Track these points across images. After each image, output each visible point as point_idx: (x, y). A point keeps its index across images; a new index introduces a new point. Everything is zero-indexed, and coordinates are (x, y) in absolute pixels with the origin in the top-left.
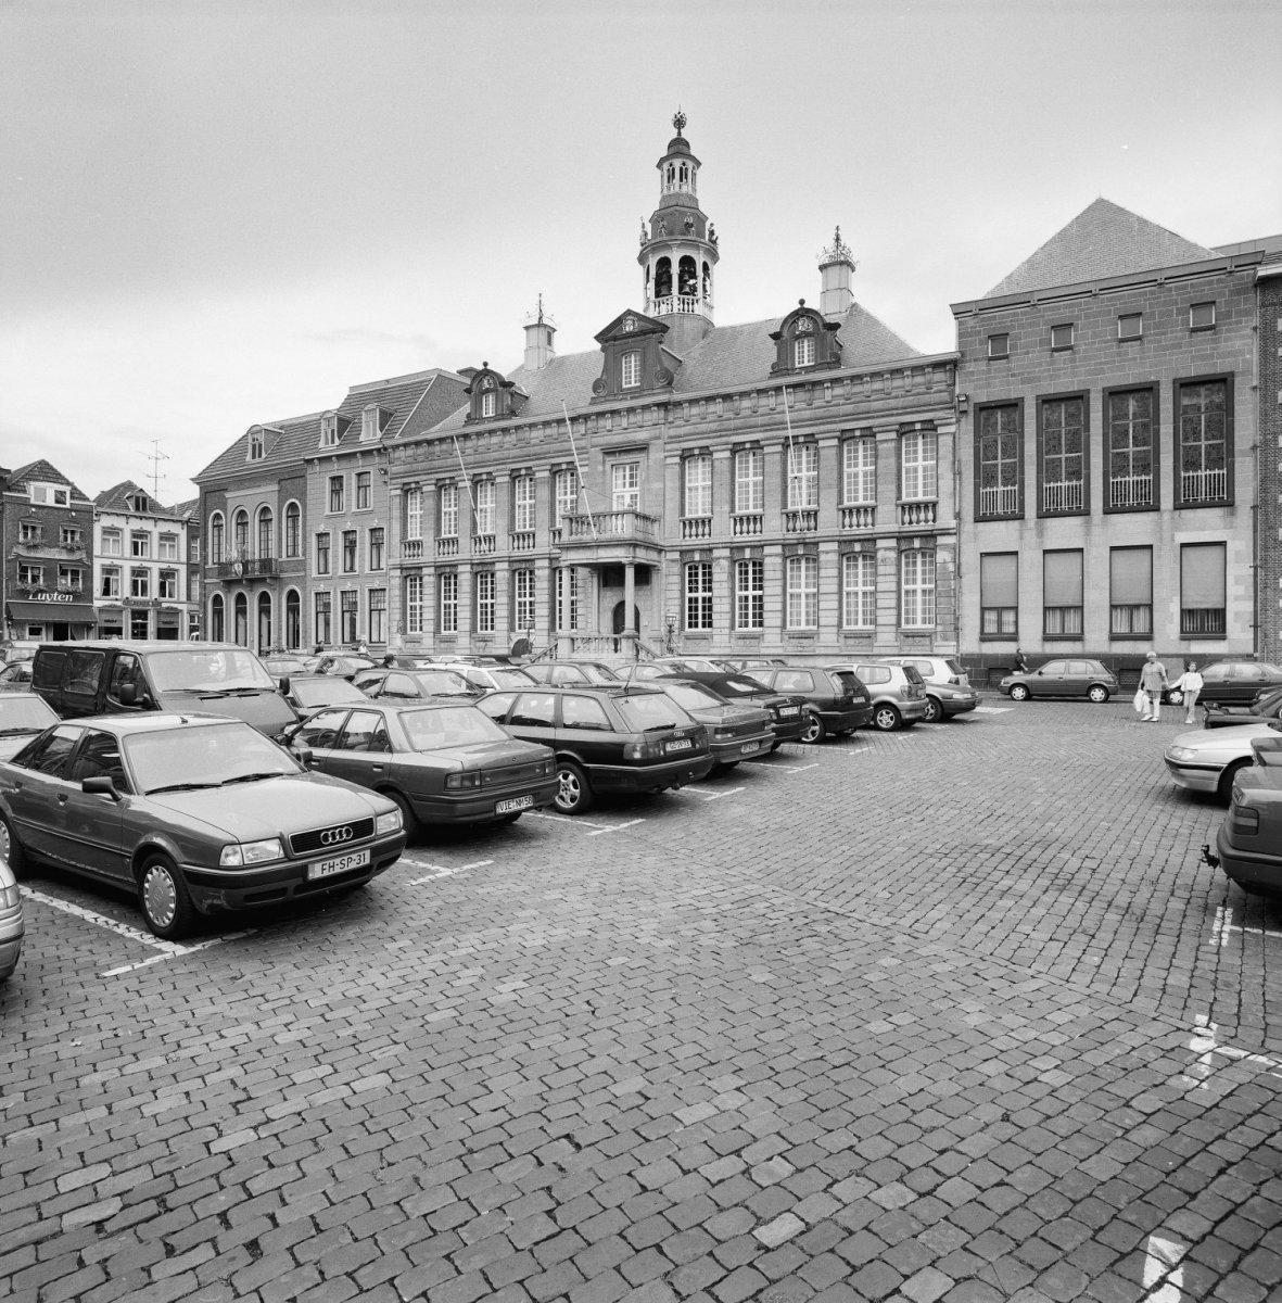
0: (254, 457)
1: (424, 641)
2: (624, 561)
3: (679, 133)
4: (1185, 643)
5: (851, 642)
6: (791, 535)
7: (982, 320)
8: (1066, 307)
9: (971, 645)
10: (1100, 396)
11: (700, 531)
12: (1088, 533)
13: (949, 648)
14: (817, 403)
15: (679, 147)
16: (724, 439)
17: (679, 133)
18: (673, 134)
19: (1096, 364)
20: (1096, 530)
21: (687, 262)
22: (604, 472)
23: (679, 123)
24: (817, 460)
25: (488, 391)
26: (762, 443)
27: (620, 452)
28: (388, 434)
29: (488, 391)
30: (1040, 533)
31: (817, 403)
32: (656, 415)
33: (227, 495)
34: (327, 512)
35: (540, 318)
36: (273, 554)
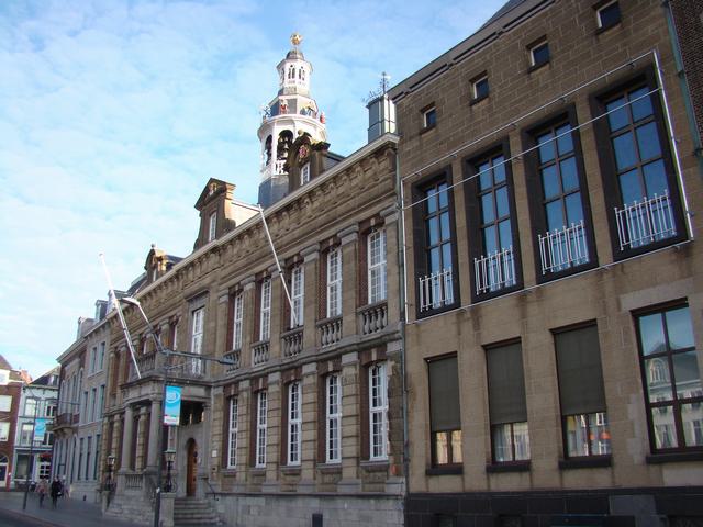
4: (654, 469)
7: (415, 97)
8: (479, 56)
9: (418, 483)
10: (586, 104)
12: (524, 316)
13: (397, 487)
14: (303, 220)
16: (249, 272)
19: (512, 105)
27: (196, 298)
31: (303, 220)
32: (214, 258)
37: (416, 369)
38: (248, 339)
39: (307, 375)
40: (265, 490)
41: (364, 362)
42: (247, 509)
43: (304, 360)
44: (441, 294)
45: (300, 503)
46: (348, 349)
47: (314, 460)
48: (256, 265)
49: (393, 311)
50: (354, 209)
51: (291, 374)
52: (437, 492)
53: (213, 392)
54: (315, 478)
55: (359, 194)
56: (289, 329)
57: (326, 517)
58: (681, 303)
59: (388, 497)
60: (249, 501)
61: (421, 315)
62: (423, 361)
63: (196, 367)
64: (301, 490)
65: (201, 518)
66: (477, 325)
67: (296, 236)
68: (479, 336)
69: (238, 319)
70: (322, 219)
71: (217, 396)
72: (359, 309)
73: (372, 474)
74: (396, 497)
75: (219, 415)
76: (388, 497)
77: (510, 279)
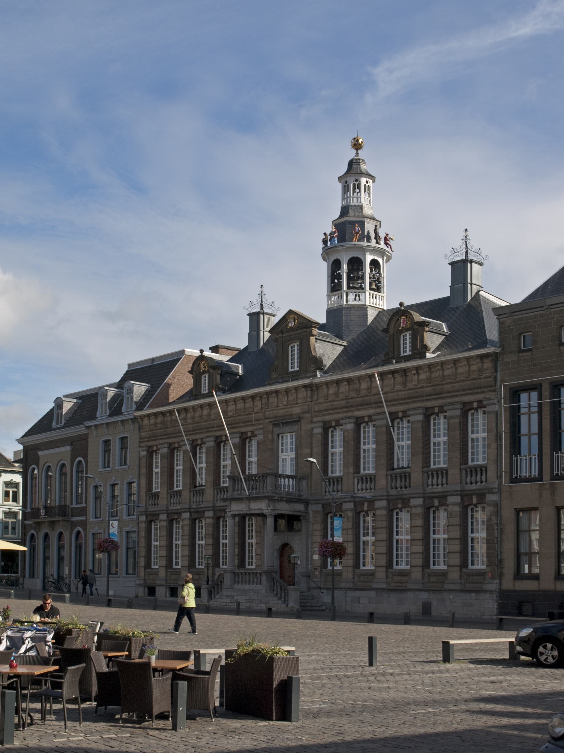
0: (57, 424)
1: (344, 574)
2: (265, 512)
3: (357, 154)
5: (433, 579)
6: (393, 492)
9: (508, 584)
11: (473, 479)
14: (410, 385)
15: (353, 166)
16: (350, 414)
17: (357, 154)
18: (351, 154)
21: (356, 264)
22: (272, 440)
23: (357, 146)
25: (204, 372)
26: (445, 408)
29: (204, 372)
30: (271, 515)
31: (410, 385)
33: (40, 453)
34: (100, 469)
36: (68, 503)
37: (508, 514)
38: (351, 470)
40: (374, 586)
41: (149, 520)
42: (358, 600)
43: (378, 498)
44: (528, 466)
45: (410, 594)
46: (454, 493)
47: (461, 566)
48: (358, 410)
49: (491, 472)
50: (459, 391)
51: (397, 503)
52: (521, 589)
53: (312, 508)
54: (423, 579)
55: (464, 381)
56: (393, 469)
57: (434, 604)
58: (536, 509)
59: (485, 591)
60: (358, 593)
61: (515, 480)
62: (513, 510)
63: (288, 485)
64: (410, 586)
65: (306, 603)
66: (553, 494)
69: (157, 470)
70: (428, 390)
71: (315, 512)
72: (425, 469)
73: (471, 577)
74: (491, 592)
75: (318, 526)
76: (485, 591)
77: (535, 473)
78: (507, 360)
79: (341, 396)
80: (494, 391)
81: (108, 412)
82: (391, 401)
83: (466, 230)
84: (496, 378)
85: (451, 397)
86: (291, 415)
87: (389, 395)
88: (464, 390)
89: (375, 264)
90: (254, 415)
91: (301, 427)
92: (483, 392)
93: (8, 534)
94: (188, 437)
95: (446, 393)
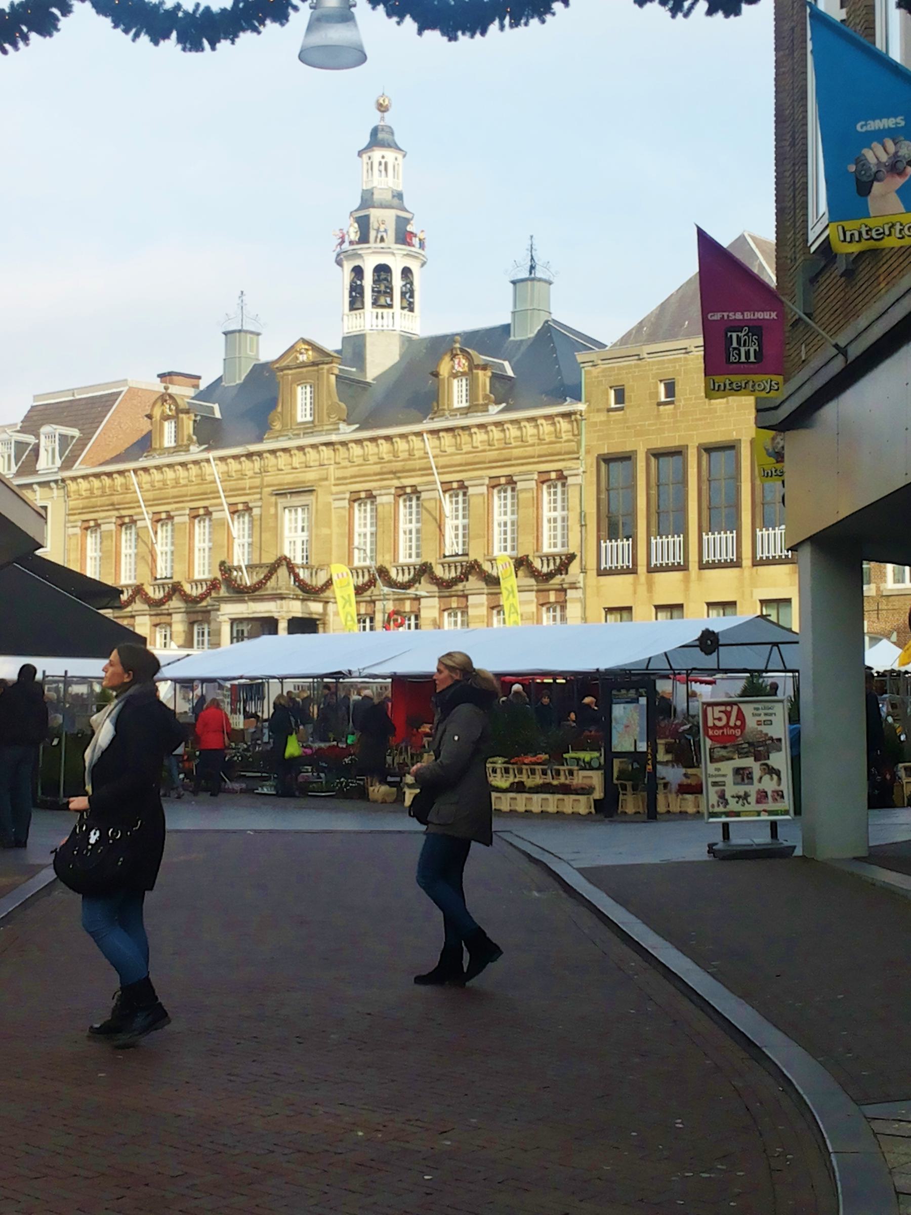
3: (382, 119)
12: (687, 589)
17: (382, 119)
18: (375, 118)
20: (694, 585)
21: (382, 271)
23: (382, 108)
24: (516, 504)
28: (68, 464)
35: (532, 268)
39: (476, 606)
50: (533, 457)
67: (458, 462)
68: (651, 598)
77: (628, 563)
78: (595, 420)
79: (373, 459)
80: (578, 459)
81: (58, 462)
82: (442, 467)
83: (532, 237)
84: (579, 443)
85: (522, 464)
86: (304, 482)
87: (440, 459)
88: (539, 456)
89: (406, 272)
90: (248, 481)
91: (317, 498)
92: (563, 460)
93: (903, 582)
94: (148, 509)
95: (516, 459)
